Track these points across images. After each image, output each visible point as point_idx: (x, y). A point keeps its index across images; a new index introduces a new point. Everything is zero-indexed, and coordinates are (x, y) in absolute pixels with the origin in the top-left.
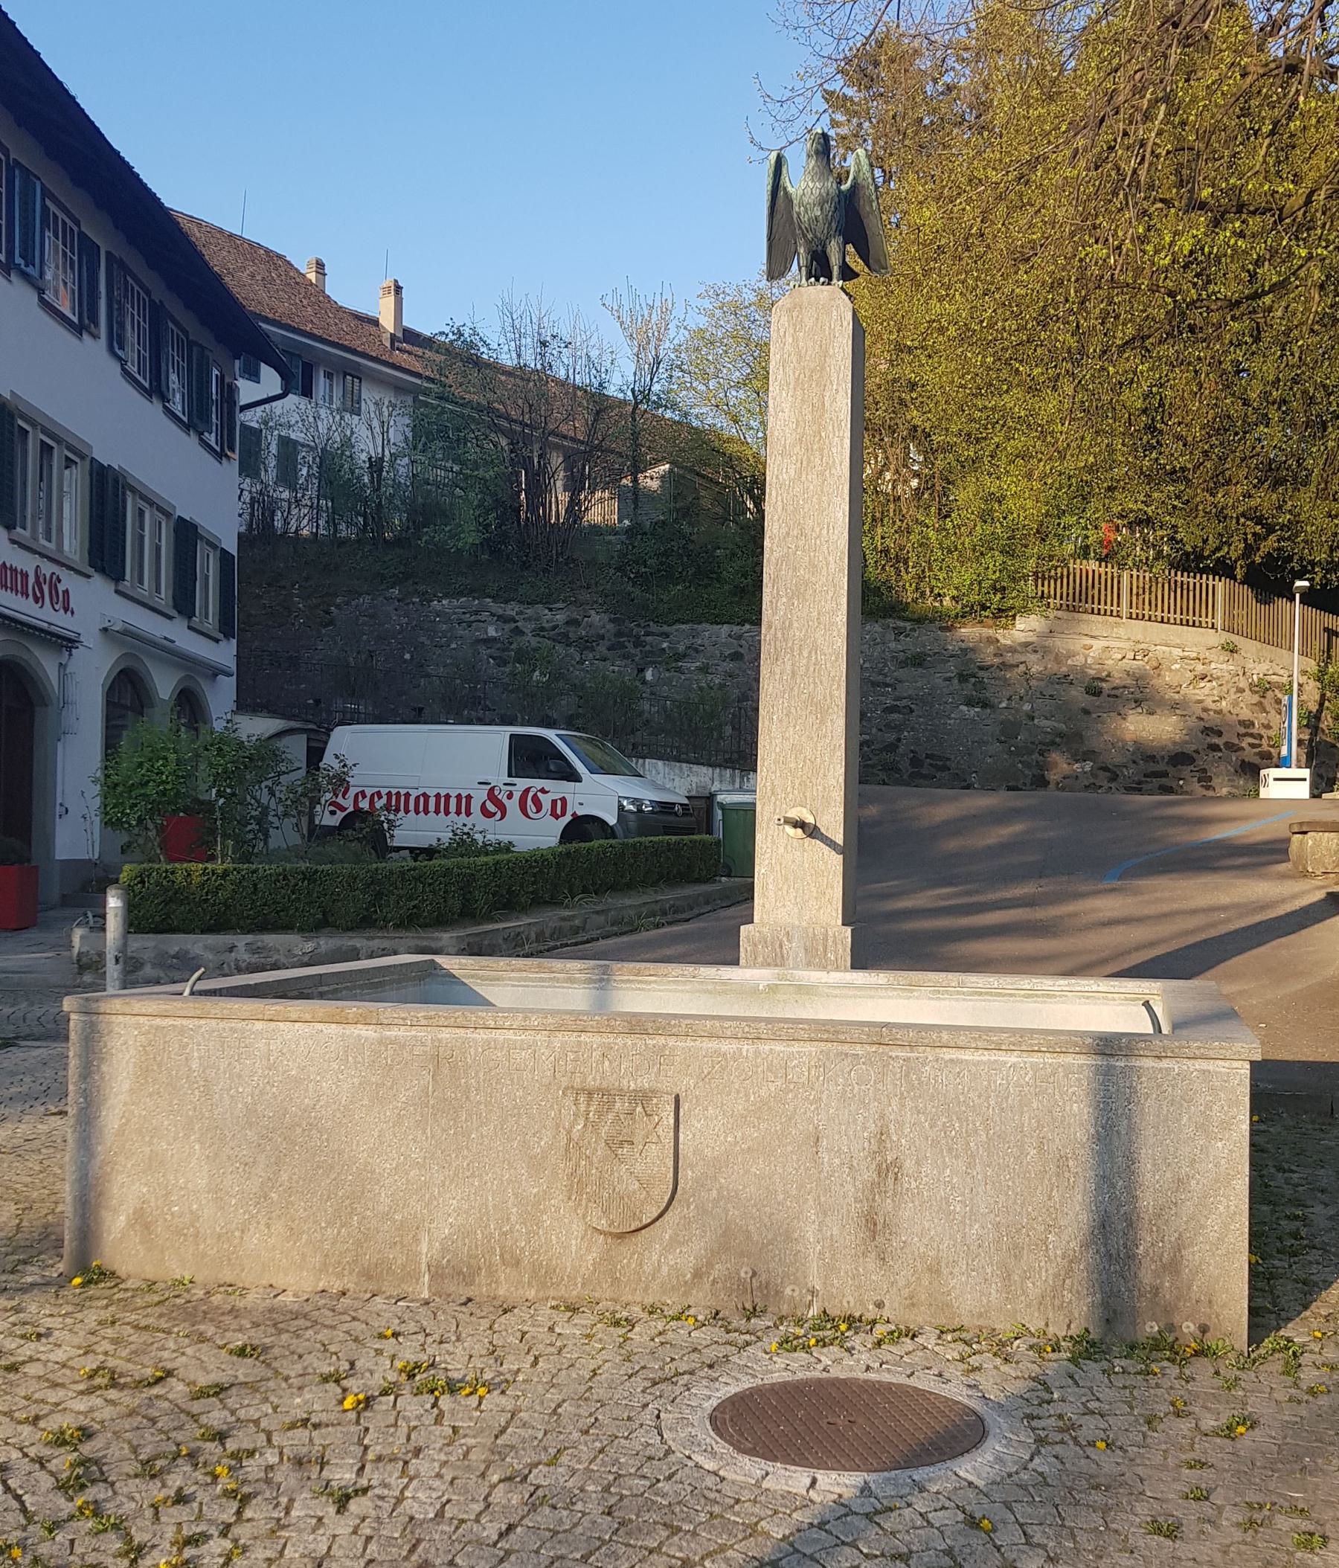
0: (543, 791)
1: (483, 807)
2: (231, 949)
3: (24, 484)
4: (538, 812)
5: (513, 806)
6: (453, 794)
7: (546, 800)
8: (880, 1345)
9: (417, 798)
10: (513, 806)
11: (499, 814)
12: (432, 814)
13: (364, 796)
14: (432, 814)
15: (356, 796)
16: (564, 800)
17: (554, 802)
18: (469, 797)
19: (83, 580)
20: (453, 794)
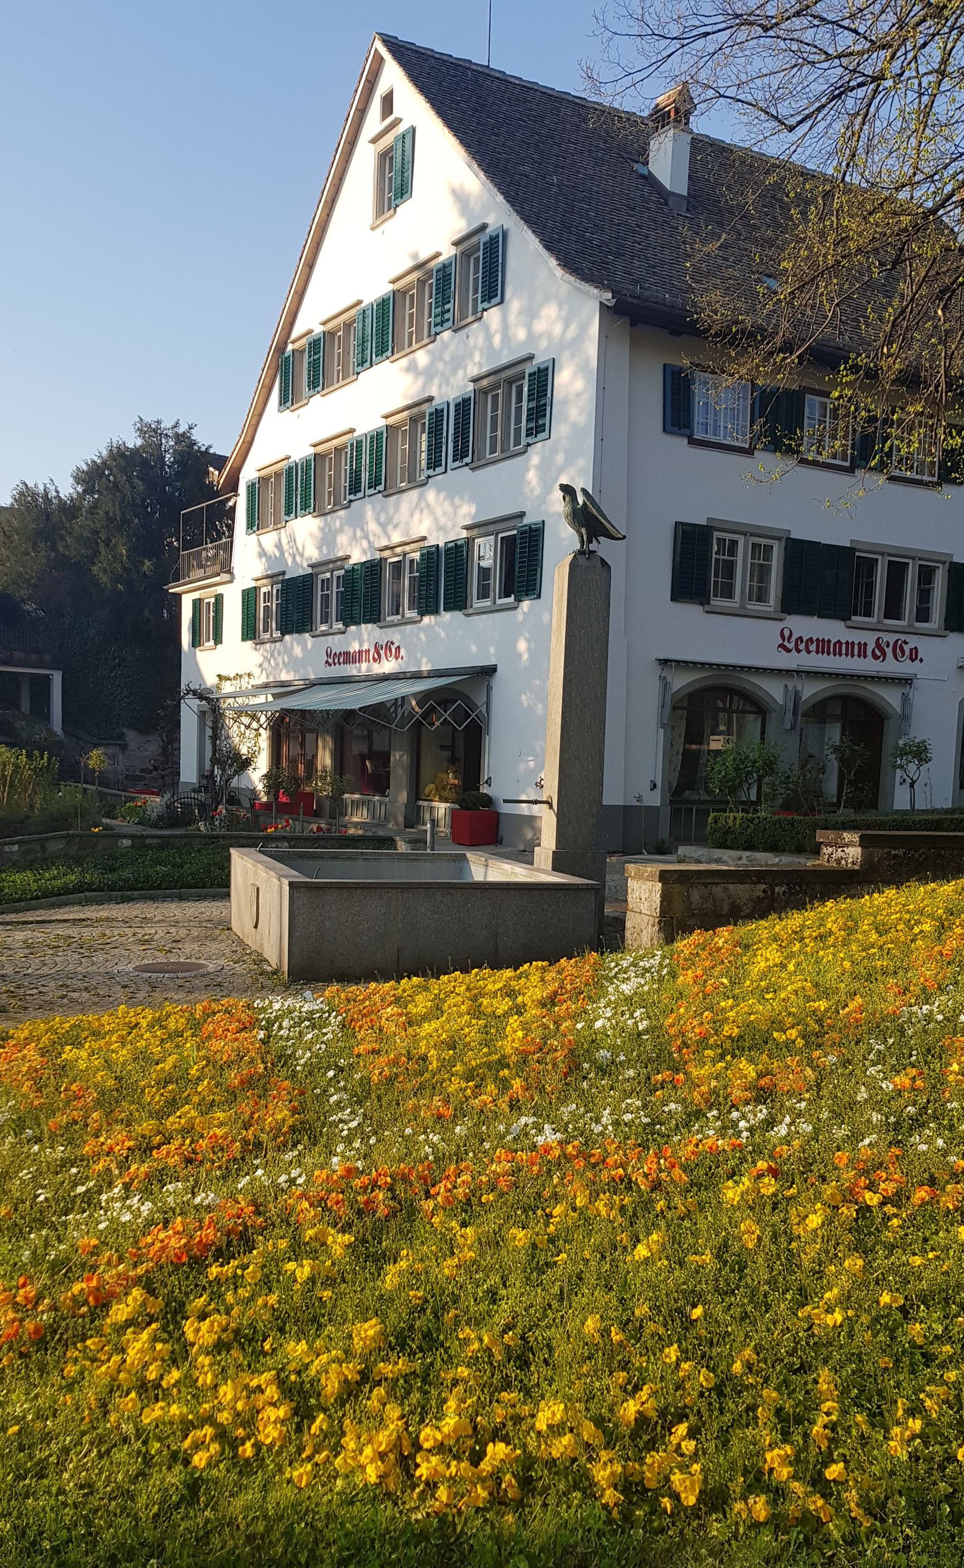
0: (906, 643)
1: (873, 651)
2: (740, 858)
3: (501, 570)
4: (903, 656)
5: (889, 651)
6: (856, 657)
7: (907, 648)
8: (802, 1366)
9: (835, 644)
10: (889, 651)
11: (881, 659)
12: (844, 656)
13: (802, 641)
14: (844, 656)
15: (797, 640)
16: (916, 648)
17: (911, 650)
18: (865, 644)
19: (457, 236)
20: (856, 657)
